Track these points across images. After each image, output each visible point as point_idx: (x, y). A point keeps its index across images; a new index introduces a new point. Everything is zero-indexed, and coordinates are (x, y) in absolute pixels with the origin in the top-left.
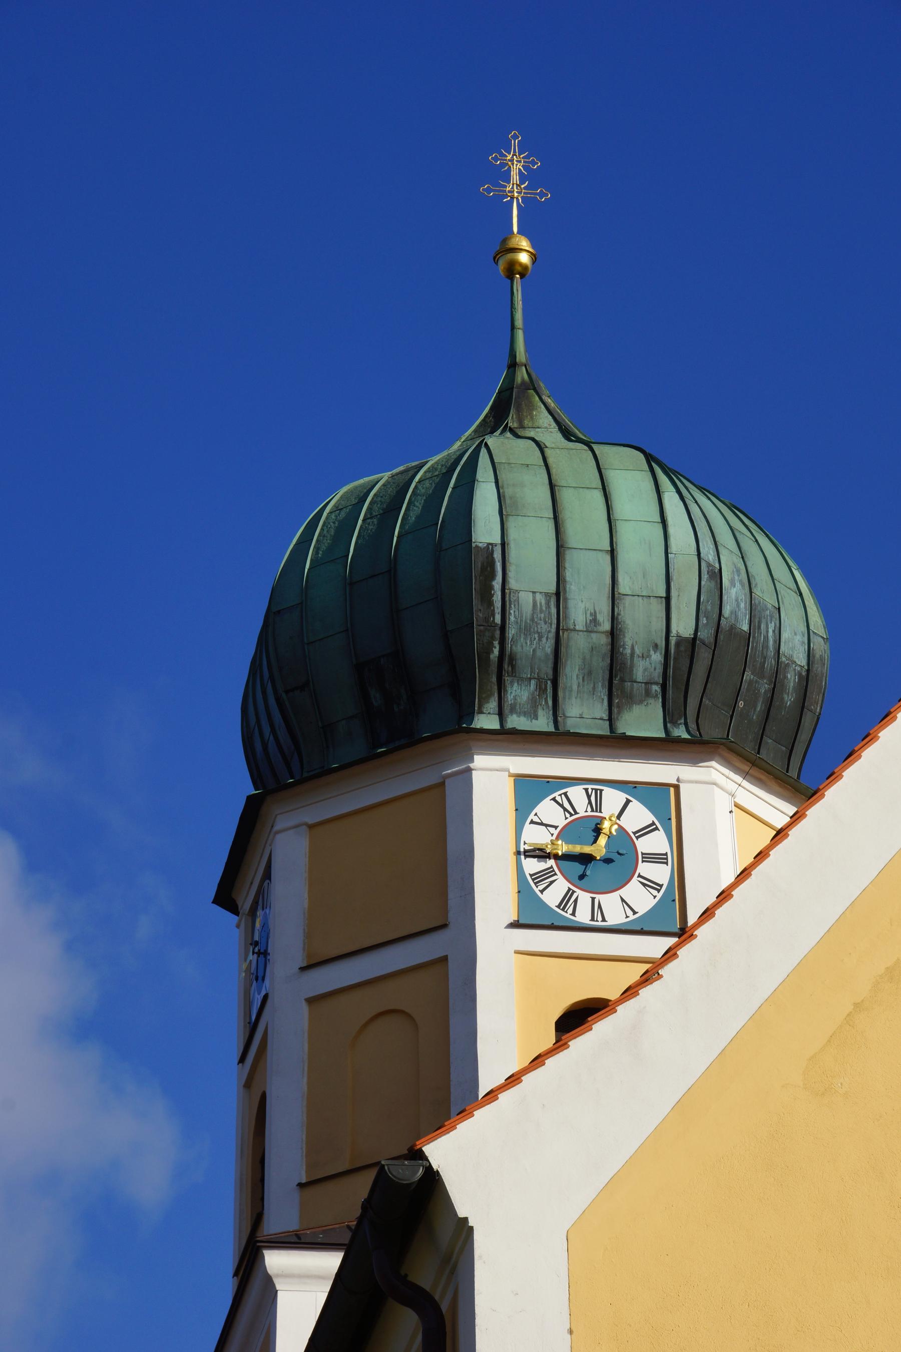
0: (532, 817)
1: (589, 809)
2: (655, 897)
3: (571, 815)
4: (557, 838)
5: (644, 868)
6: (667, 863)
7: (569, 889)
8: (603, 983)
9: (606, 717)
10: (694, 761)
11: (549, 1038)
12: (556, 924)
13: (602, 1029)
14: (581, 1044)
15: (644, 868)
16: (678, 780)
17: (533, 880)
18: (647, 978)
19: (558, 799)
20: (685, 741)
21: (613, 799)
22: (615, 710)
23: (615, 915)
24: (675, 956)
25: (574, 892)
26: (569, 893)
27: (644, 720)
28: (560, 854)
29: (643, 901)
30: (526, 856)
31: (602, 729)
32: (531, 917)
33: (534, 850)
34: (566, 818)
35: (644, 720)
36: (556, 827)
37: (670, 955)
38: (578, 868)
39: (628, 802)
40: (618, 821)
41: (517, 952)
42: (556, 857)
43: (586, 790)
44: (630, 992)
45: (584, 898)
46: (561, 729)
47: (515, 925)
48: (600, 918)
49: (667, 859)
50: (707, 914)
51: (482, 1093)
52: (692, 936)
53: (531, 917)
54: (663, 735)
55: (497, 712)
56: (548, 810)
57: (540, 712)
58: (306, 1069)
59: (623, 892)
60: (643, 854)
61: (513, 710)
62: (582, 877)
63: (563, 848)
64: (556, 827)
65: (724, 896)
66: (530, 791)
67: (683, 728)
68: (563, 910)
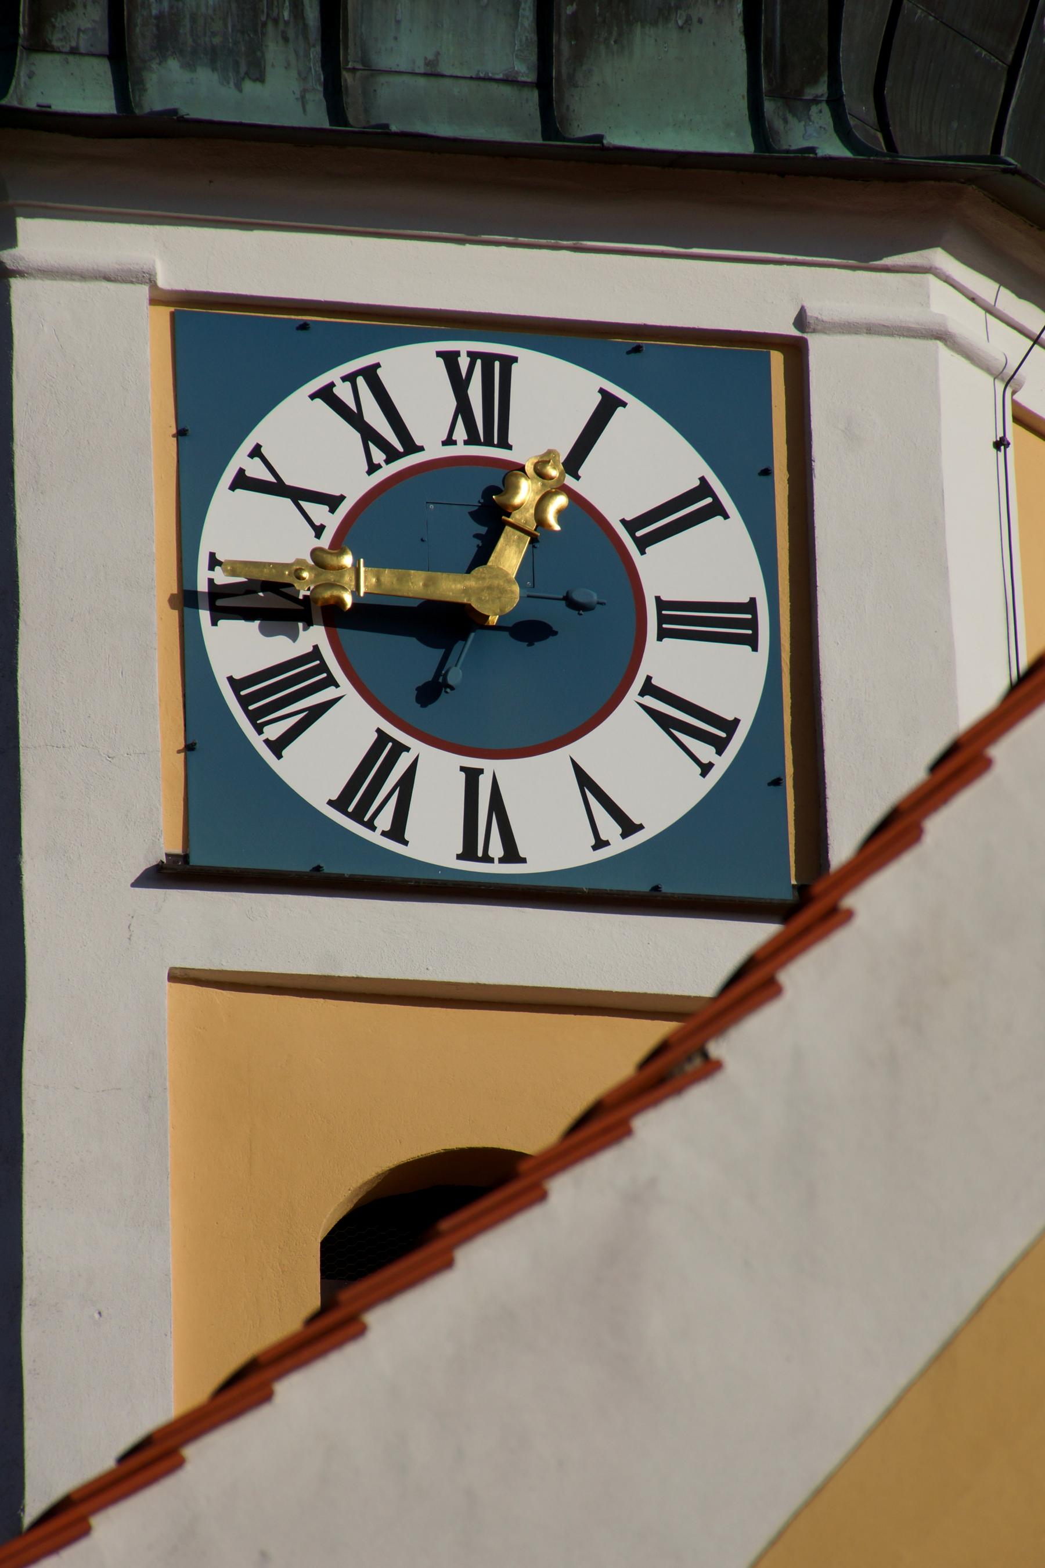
0: (240, 460)
1: (460, 433)
2: (706, 769)
3: (392, 455)
4: (338, 545)
5: (667, 661)
6: (752, 642)
7: (382, 738)
8: (501, 1092)
9: (525, 70)
10: (864, 250)
11: (299, 1291)
12: (329, 869)
13: (492, 1263)
14: (410, 1323)
15: (667, 661)
16: (801, 321)
17: (244, 702)
18: (664, 1074)
19: (344, 392)
20: (831, 168)
21: (551, 397)
22: (563, 46)
23: (553, 835)
24: (770, 989)
25: (400, 748)
26: (382, 753)
27: (670, 91)
28: (348, 599)
29: (656, 780)
30: (218, 614)
31: (514, 123)
32: (236, 837)
33: (248, 589)
34: (373, 468)
35: (670, 91)
36: (333, 502)
37: (751, 985)
38: (416, 658)
39: (608, 405)
40: (569, 481)
41: (178, 976)
42: (334, 616)
43: (450, 359)
44: (600, 1125)
45: (438, 775)
46: (356, 119)
47: (171, 873)
48: (496, 849)
49: (753, 624)
50: (895, 832)
51: (34, 1506)
52: (835, 917)
53: (236, 837)
54: (745, 146)
55: (104, 47)
56: (304, 437)
57: (274, 52)
58: (984, 286)
59: (586, 750)
60: (661, 604)
61: (166, 40)
62: (430, 692)
63: (358, 581)
64: (333, 502)
65: (960, 763)
66: (230, 362)
67: (822, 117)
68: (357, 816)
